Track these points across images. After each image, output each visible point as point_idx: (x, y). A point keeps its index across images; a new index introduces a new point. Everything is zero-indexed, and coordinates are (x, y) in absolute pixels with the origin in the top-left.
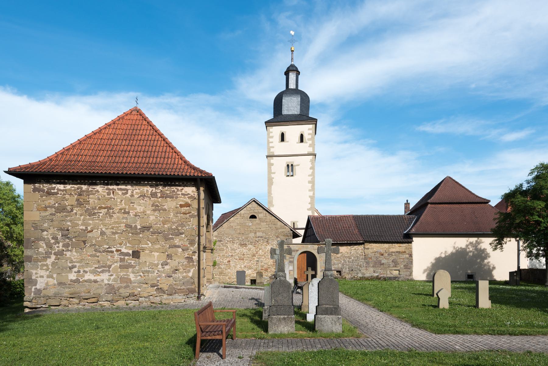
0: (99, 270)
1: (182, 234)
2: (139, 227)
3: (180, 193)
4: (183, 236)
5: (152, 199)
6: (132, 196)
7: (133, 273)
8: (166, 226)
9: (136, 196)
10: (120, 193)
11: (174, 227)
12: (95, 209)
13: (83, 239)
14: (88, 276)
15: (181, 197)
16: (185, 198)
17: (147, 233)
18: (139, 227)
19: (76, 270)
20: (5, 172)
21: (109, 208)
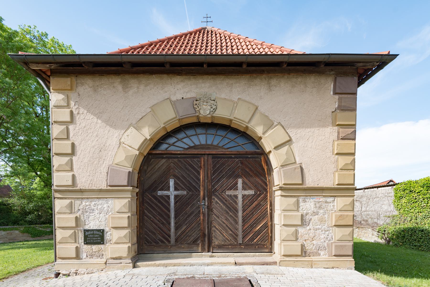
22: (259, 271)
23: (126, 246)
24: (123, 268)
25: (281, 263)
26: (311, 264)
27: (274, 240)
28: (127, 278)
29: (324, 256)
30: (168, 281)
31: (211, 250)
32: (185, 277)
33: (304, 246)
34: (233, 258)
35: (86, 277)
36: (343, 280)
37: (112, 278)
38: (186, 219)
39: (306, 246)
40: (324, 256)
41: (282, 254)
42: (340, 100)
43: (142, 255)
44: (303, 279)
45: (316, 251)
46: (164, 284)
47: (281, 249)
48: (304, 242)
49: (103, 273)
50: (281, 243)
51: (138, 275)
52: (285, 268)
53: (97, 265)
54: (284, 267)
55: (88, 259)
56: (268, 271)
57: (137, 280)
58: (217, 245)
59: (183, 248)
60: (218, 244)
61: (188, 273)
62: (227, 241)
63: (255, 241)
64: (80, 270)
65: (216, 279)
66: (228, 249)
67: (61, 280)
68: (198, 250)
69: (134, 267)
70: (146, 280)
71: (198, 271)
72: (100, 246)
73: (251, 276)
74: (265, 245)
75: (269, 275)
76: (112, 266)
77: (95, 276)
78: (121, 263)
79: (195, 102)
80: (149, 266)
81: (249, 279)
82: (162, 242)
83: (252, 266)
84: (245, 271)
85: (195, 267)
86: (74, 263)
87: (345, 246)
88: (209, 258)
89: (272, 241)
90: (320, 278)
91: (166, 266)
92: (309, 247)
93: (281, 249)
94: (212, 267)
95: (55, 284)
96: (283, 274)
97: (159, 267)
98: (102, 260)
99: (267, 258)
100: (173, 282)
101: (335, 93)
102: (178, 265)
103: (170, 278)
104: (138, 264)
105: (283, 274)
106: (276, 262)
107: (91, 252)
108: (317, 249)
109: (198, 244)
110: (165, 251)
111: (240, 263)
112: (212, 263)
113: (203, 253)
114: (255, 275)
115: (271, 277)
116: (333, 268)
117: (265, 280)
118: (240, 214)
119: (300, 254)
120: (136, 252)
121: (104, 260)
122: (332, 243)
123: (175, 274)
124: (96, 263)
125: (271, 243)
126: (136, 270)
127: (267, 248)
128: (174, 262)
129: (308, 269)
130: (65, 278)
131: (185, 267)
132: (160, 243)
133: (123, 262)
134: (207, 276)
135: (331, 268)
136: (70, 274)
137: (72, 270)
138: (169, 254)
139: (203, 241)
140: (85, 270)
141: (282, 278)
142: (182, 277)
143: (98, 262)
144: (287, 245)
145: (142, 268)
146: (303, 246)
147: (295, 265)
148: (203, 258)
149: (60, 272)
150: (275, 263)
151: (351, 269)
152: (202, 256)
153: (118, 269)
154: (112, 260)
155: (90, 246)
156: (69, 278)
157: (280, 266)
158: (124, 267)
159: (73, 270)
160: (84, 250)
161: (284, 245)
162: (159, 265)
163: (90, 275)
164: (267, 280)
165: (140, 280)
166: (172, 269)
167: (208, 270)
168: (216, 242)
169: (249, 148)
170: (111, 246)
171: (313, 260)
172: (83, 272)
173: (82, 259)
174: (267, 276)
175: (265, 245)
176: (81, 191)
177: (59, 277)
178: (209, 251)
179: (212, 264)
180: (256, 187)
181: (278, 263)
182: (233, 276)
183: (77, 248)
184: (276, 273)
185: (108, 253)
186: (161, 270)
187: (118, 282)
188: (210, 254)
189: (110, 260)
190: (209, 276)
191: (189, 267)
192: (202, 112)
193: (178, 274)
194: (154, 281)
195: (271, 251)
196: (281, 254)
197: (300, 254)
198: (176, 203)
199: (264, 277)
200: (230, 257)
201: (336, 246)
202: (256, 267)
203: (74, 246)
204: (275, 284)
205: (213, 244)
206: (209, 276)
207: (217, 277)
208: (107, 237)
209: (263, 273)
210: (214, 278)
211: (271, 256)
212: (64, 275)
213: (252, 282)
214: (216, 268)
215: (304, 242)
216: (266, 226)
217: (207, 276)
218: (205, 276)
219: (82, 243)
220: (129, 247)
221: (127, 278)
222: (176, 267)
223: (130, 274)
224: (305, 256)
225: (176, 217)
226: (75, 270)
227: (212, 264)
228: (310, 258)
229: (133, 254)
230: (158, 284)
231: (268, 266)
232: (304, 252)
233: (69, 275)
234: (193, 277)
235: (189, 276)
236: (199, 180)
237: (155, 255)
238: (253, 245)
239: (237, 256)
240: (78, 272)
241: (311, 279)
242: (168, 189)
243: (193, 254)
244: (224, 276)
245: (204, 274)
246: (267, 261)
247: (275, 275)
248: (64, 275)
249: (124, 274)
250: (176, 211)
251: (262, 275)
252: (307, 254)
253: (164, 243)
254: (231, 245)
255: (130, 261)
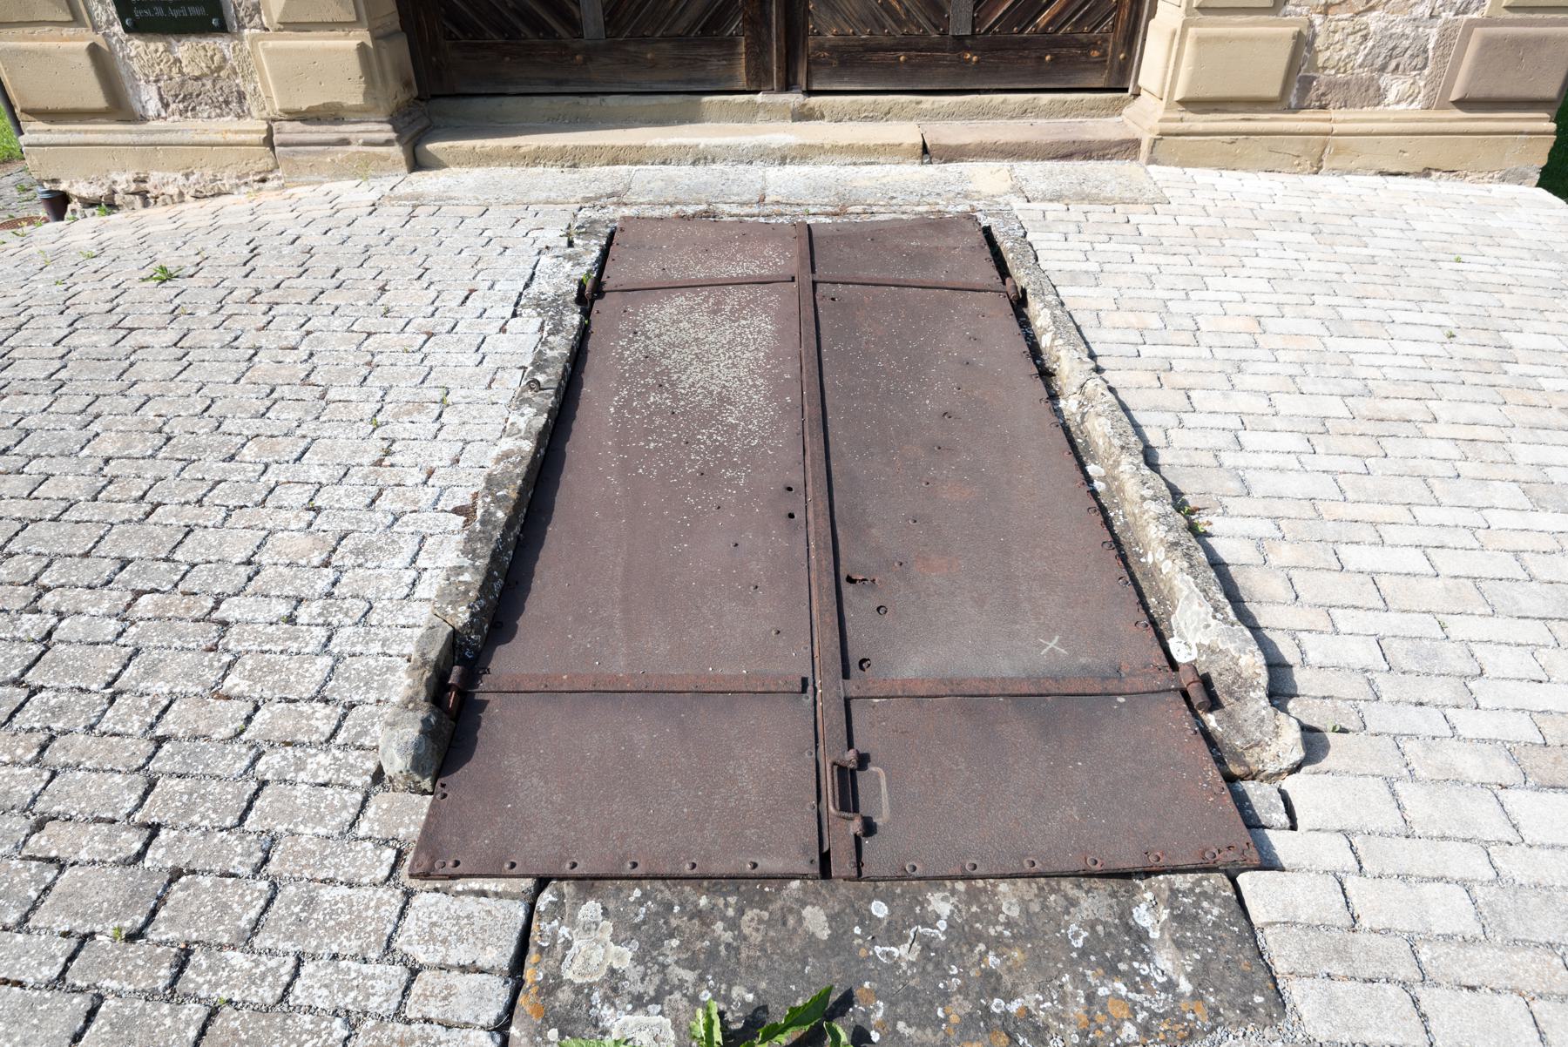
22: (1043, 187)
23: (349, 43)
24: (362, 170)
25: (1160, 145)
26: (1317, 150)
27: (1152, 14)
28: (391, 217)
29: (1402, 103)
30: (587, 229)
31: (802, 78)
32: (669, 211)
33: (1310, 44)
34: (912, 125)
35: (195, 213)
36: (1461, 230)
37: (315, 214)
39: (1319, 43)
40: (1403, 106)
41: (1178, 97)
43: (445, 104)
44: (1255, 224)
45: (1365, 74)
46: (571, 244)
47: (1177, 64)
48: (1318, 20)
49: (269, 196)
50: (1185, 25)
51: (441, 201)
52: (1178, 170)
53: (231, 154)
54: (1173, 169)
55: (174, 122)
56: (1086, 189)
57: (435, 222)
58: (834, 49)
59: (653, 65)
60: (839, 41)
61: (682, 197)
62: (889, 22)
63: (1043, 19)
64: (155, 177)
65: (817, 224)
66: (891, 69)
67: (81, 230)
68: (732, 78)
69: (417, 163)
70: (481, 223)
71: (735, 189)
72: (210, 43)
73: (994, 209)
74: (1093, 45)
75: (1086, 207)
76: (303, 157)
77: (236, 206)
78: (345, 142)
80: (487, 159)
81: (985, 223)
82: (539, 26)
83: (1005, 165)
84: (971, 187)
85: (718, 167)
86: (110, 139)
87: (1541, 41)
88: (789, 124)
89: (1138, 16)
90: (1346, 221)
91: (573, 160)
92: (1339, 50)
93: (1177, 64)
94: (805, 169)
95: (58, 245)
96: (1157, 201)
97: (540, 169)
98: (247, 123)
99: (1090, 122)
100: (612, 235)
102: (634, 156)
103: (595, 215)
104: (430, 147)
105: (1157, 201)
106: (1136, 143)
107: (177, 78)
108: (1379, 62)
109: (732, 43)
110: (559, 83)
111: (947, 148)
112: (803, 146)
113: (759, 98)
114: (1018, 204)
115: (1098, 213)
116: (1426, 173)
117: (1062, 228)
119: (1274, 91)
120: (407, 85)
121: (254, 127)
122: (1472, 24)
123: (617, 197)
124: (219, 138)
125: (1132, 36)
126: (426, 182)
127: (1101, 63)
128: (609, 142)
129: (1294, 178)
130: (95, 219)
131: (670, 170)
132: (525, 31)
133: (352, 137)
134: (776, 208)
135: (1417, 175)
136: (118, 200)
137: (114, 176)
138: (583, 100)
139: (757, 24)
140: (181, 180)
141: (1152, 218)
142: (657, 213)
143: (231, 138)
144: (1219, 39)
145: (454, 169)
146: (1303, 44)
147: (1230, 155)
148: (759, 125)
149: (63, 187)
150: (1128, 148)
151: (1521, 179)
152: (750, 114)
153: (339, 173)
154: (298, 125)
155: (161, 46)
156: (116, 217)
157: (1152, 161)
158: (367, 161)
159: (124, 181)
160: (136, 66)
161: (1200, 41)
162: (536, 158)
163: (212, 204)
164: (1072, 228)
165: (450, 226)
166: (602, 177)
167: (783, 182)
168: (827, 30)
170: (270, 44)
171: (1337, 128)
172: (172, 190)
173: (144, 119)
174: (1077, 210)
175: (1093, 45)
177: (68, 214)
178: (787, 87)
179: (801, 155)
181: (1145, 147)
182: (908, 208)
183: (94, 50)
184: (1128, 195)
185: (265, 86)
186: (550, 178)
187: (346, 232)
188: (794, 99)
189: (288, 126)
190: (789, 210)
191: (686, 169)
193: (634, 198)
194: (521, 229)
195: (1120, 82)
196: (1171, 92)
197: (1274, 91)
199: (1064, 215)
200: (898, 117)
201: (1488, 44)
202: (1025, 168)
203: (76, 43)
204: (1111, 246)
205: (811, 42)
206: (789, 210)
207: (827, 215)
209: (1057, 198)
210: (810, 221)
211: (1116, 109)
212: (90, 203)
213: (999, 238)
214: (825, 172)
215: (1318, 20)
217: (776, 208)
218: (768, 209)
219: (110, 23)
220: (362, 48)
221: (391, 217)
222: (622, 169)
223: (400, 198)
224: (1299, 108)
226: (130, 176)
227: (801, 155)
228: (1322, 115)
229: (394, 93)
230: (540, 244)
231: (1092, 163)
232: (1300, 82)
233: (112, 206)
234: (709, 215)
235: (690, 210)
237: (509, 104)
238: (1025, 44)
239: (935, 115)
240: (148, 186)
241: (1297, 226)
243: (706, 99)
244: (859, 209)
245: (762, 201)
246: (1088, 137)
247: (1119, 208)
248: (90, 203)
249: (373, 196)
251: (1055, 205)
252: (1313, 95)
253: (550, 33)
254: (906, 47)
255: (386, 132)
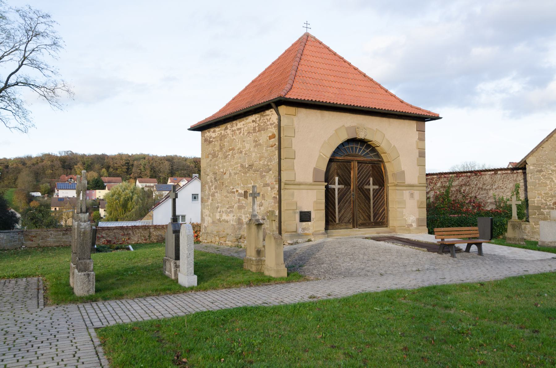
0: (229, 210)
1: (270, 170)
2: (247, 166)
3: (268, 123)
4: (271, 172)
5: (254, 134)
6: (243, 134)
7: (244, 214)
8: (261, 162)
9: (246, 134)
10: (238, 132)
11: (266, 163)
12: (227, 151)
13: (222, 181)
14: (224, 217)
15: (269, 128)
16: (272, 128)
17: (251, 171)
18: (247, 166)
19: (219, 210)
20: (189, 129)
21: (233, 149)
38: (344, 205)
42: (419, 134)
79: (356, 129)
101: (417, 131)
118: (372, 202)
169: (372, 157)
176: (299, 184)
180: (380, 186)
192: (360, 136)
198: (338, 194)
208: (313, 216)
216: (384, 210)
225: (338, 204)
236: (350, 178)
242: (334, 184)
250: (338, 199)
